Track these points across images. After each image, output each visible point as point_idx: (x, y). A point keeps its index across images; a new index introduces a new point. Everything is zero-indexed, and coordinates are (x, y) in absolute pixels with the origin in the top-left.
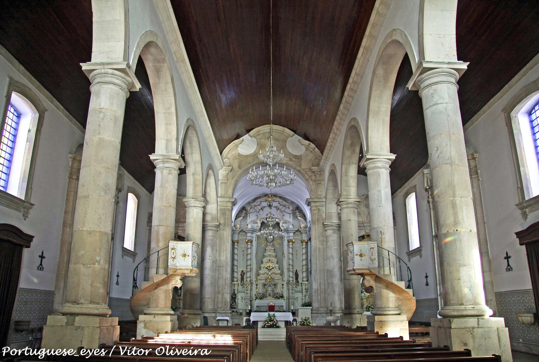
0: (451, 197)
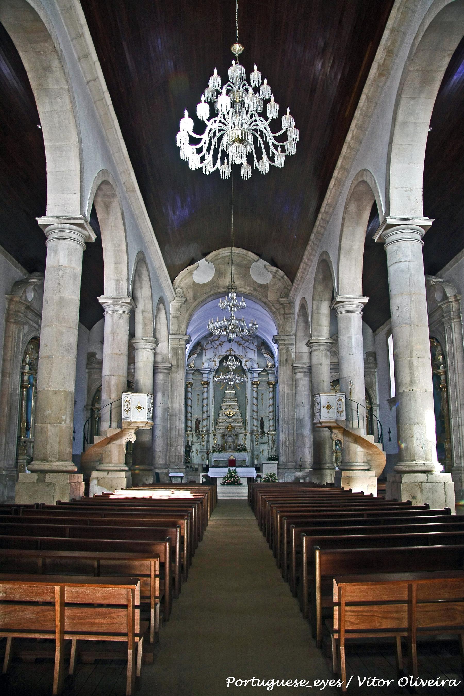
0: (408, 357)
